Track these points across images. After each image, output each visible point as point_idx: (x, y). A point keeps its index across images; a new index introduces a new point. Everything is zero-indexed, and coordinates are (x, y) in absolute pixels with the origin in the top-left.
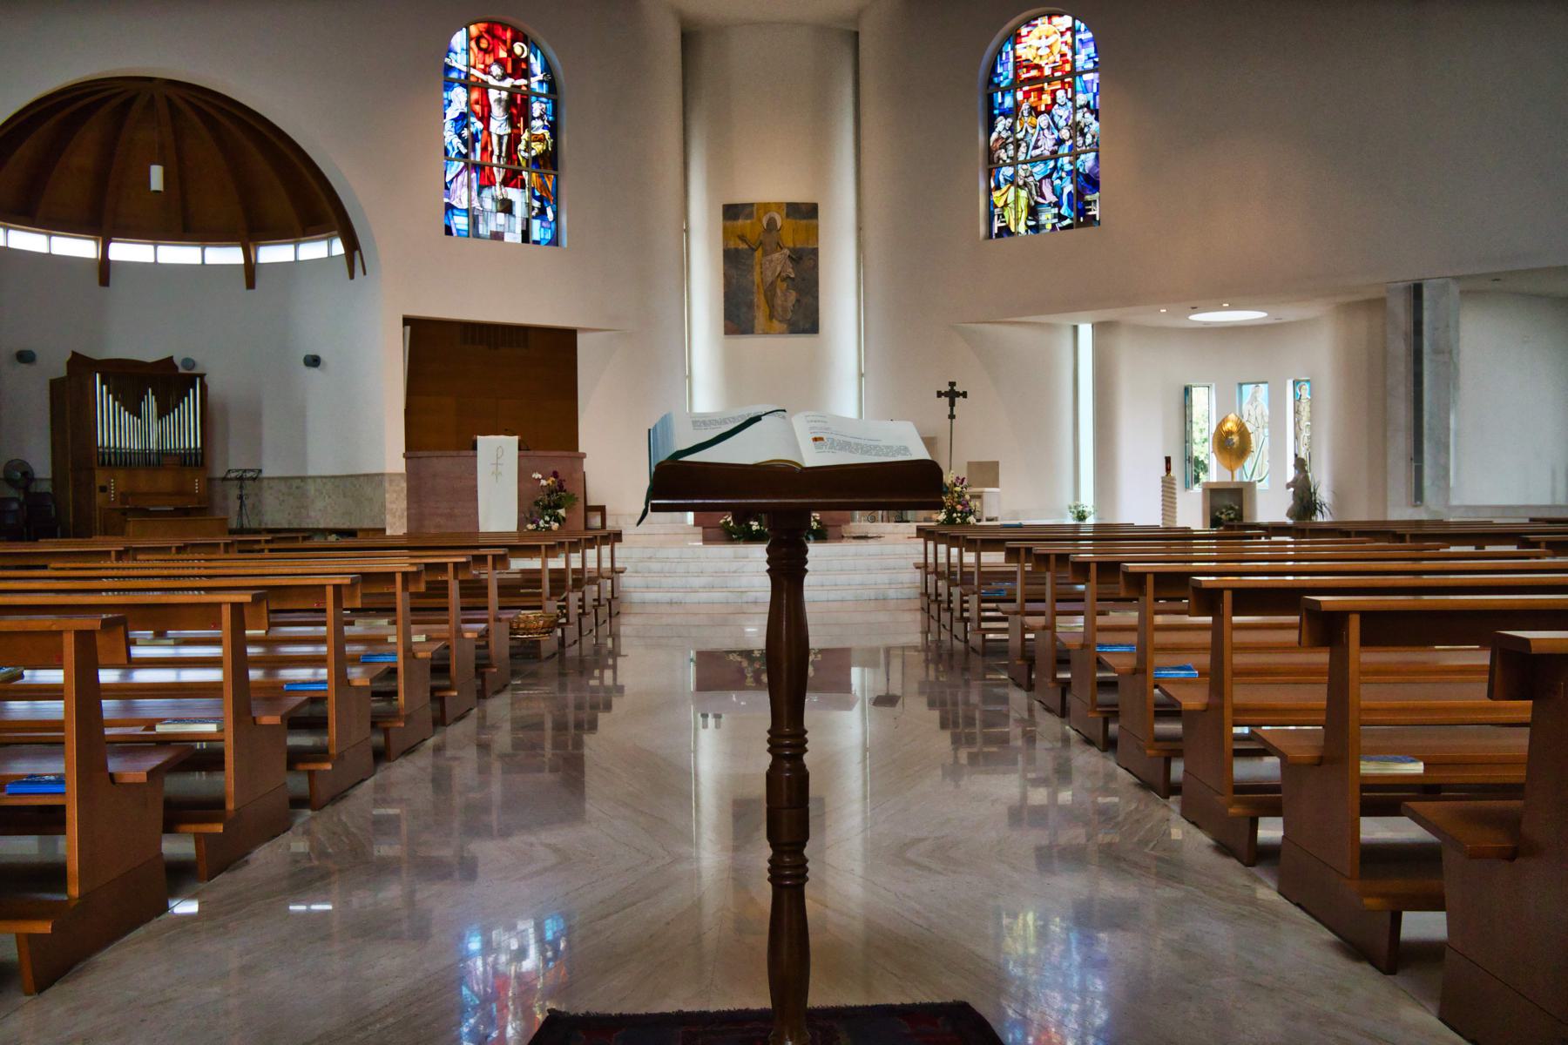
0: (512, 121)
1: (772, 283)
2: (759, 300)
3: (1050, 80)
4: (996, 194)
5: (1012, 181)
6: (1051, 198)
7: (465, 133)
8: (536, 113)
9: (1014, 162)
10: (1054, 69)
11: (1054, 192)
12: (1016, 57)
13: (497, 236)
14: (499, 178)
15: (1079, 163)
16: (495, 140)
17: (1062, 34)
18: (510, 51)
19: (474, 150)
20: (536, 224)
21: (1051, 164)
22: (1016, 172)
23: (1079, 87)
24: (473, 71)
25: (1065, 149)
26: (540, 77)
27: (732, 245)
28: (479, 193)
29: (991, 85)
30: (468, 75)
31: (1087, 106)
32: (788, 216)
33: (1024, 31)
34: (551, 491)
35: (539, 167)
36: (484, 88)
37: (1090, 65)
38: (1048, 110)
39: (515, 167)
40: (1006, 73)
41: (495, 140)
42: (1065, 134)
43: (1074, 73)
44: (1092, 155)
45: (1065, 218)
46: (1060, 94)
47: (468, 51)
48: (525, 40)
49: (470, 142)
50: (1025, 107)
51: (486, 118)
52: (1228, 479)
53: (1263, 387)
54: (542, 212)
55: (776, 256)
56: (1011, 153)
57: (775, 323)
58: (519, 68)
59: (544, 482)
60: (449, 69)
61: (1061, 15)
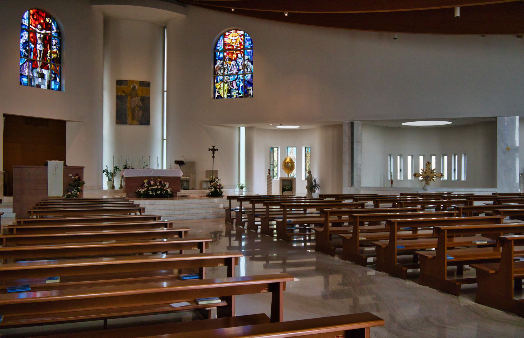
0: (45, 45)
1: (133, 108)
2: (129, 113)
3: (236, 50)
4: (217, 84)
5: (222, 81)
6: (235, 87)
7: (27, 48)
8: (54, 44)
9: (223, 75)
10: (237, 47)
11: (237, 85)
12: (224, 42)
13: (39, 86)
14: (39, 66)
15: (245, 77)
16: (38, 51)
17: (240, 36)
18: (45, 21)
19: (31, 55)
20: (53, 83)
21: (236, 77)
22: (224, 78)
23: (246, 53)
24: (31, 26)
25: (241, 72)
26: (55, 31)
27: (119, 94)
28: (32, 70)
29: (215, 50)
30: (29, 27)
31: (249, 59)
32: (140, 85)
33: (227, 34)
34: (75, 181)
35: (54, 62)
36: (35, 33)
37: (250, 47)
38: (235, 59)
39: (46, 62)
40: (220, 46)
41: (38, 51)
42: (241, 67)
43: (245, 49)
44: (250, 75)
45: (240, 94)
46: (239, 55)
47: (29, 19)
48: (50, 17)
49: (29, 52)
50: (227, 58)
51: (35, 43)
52: (287, 177)
53: (295, 149)
54: (55, 79)
55: (136, 99)
56: (222, 72)
57: (135, 121)
58: (48, 27)
59: (73, 177)
60: (23, 25)
61: (240, 30)
